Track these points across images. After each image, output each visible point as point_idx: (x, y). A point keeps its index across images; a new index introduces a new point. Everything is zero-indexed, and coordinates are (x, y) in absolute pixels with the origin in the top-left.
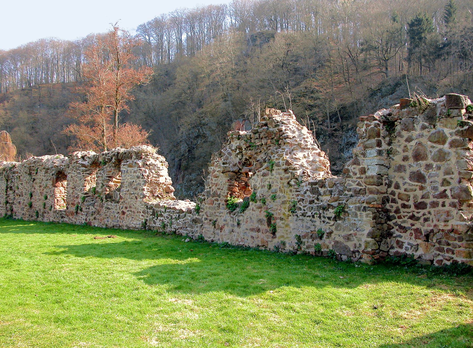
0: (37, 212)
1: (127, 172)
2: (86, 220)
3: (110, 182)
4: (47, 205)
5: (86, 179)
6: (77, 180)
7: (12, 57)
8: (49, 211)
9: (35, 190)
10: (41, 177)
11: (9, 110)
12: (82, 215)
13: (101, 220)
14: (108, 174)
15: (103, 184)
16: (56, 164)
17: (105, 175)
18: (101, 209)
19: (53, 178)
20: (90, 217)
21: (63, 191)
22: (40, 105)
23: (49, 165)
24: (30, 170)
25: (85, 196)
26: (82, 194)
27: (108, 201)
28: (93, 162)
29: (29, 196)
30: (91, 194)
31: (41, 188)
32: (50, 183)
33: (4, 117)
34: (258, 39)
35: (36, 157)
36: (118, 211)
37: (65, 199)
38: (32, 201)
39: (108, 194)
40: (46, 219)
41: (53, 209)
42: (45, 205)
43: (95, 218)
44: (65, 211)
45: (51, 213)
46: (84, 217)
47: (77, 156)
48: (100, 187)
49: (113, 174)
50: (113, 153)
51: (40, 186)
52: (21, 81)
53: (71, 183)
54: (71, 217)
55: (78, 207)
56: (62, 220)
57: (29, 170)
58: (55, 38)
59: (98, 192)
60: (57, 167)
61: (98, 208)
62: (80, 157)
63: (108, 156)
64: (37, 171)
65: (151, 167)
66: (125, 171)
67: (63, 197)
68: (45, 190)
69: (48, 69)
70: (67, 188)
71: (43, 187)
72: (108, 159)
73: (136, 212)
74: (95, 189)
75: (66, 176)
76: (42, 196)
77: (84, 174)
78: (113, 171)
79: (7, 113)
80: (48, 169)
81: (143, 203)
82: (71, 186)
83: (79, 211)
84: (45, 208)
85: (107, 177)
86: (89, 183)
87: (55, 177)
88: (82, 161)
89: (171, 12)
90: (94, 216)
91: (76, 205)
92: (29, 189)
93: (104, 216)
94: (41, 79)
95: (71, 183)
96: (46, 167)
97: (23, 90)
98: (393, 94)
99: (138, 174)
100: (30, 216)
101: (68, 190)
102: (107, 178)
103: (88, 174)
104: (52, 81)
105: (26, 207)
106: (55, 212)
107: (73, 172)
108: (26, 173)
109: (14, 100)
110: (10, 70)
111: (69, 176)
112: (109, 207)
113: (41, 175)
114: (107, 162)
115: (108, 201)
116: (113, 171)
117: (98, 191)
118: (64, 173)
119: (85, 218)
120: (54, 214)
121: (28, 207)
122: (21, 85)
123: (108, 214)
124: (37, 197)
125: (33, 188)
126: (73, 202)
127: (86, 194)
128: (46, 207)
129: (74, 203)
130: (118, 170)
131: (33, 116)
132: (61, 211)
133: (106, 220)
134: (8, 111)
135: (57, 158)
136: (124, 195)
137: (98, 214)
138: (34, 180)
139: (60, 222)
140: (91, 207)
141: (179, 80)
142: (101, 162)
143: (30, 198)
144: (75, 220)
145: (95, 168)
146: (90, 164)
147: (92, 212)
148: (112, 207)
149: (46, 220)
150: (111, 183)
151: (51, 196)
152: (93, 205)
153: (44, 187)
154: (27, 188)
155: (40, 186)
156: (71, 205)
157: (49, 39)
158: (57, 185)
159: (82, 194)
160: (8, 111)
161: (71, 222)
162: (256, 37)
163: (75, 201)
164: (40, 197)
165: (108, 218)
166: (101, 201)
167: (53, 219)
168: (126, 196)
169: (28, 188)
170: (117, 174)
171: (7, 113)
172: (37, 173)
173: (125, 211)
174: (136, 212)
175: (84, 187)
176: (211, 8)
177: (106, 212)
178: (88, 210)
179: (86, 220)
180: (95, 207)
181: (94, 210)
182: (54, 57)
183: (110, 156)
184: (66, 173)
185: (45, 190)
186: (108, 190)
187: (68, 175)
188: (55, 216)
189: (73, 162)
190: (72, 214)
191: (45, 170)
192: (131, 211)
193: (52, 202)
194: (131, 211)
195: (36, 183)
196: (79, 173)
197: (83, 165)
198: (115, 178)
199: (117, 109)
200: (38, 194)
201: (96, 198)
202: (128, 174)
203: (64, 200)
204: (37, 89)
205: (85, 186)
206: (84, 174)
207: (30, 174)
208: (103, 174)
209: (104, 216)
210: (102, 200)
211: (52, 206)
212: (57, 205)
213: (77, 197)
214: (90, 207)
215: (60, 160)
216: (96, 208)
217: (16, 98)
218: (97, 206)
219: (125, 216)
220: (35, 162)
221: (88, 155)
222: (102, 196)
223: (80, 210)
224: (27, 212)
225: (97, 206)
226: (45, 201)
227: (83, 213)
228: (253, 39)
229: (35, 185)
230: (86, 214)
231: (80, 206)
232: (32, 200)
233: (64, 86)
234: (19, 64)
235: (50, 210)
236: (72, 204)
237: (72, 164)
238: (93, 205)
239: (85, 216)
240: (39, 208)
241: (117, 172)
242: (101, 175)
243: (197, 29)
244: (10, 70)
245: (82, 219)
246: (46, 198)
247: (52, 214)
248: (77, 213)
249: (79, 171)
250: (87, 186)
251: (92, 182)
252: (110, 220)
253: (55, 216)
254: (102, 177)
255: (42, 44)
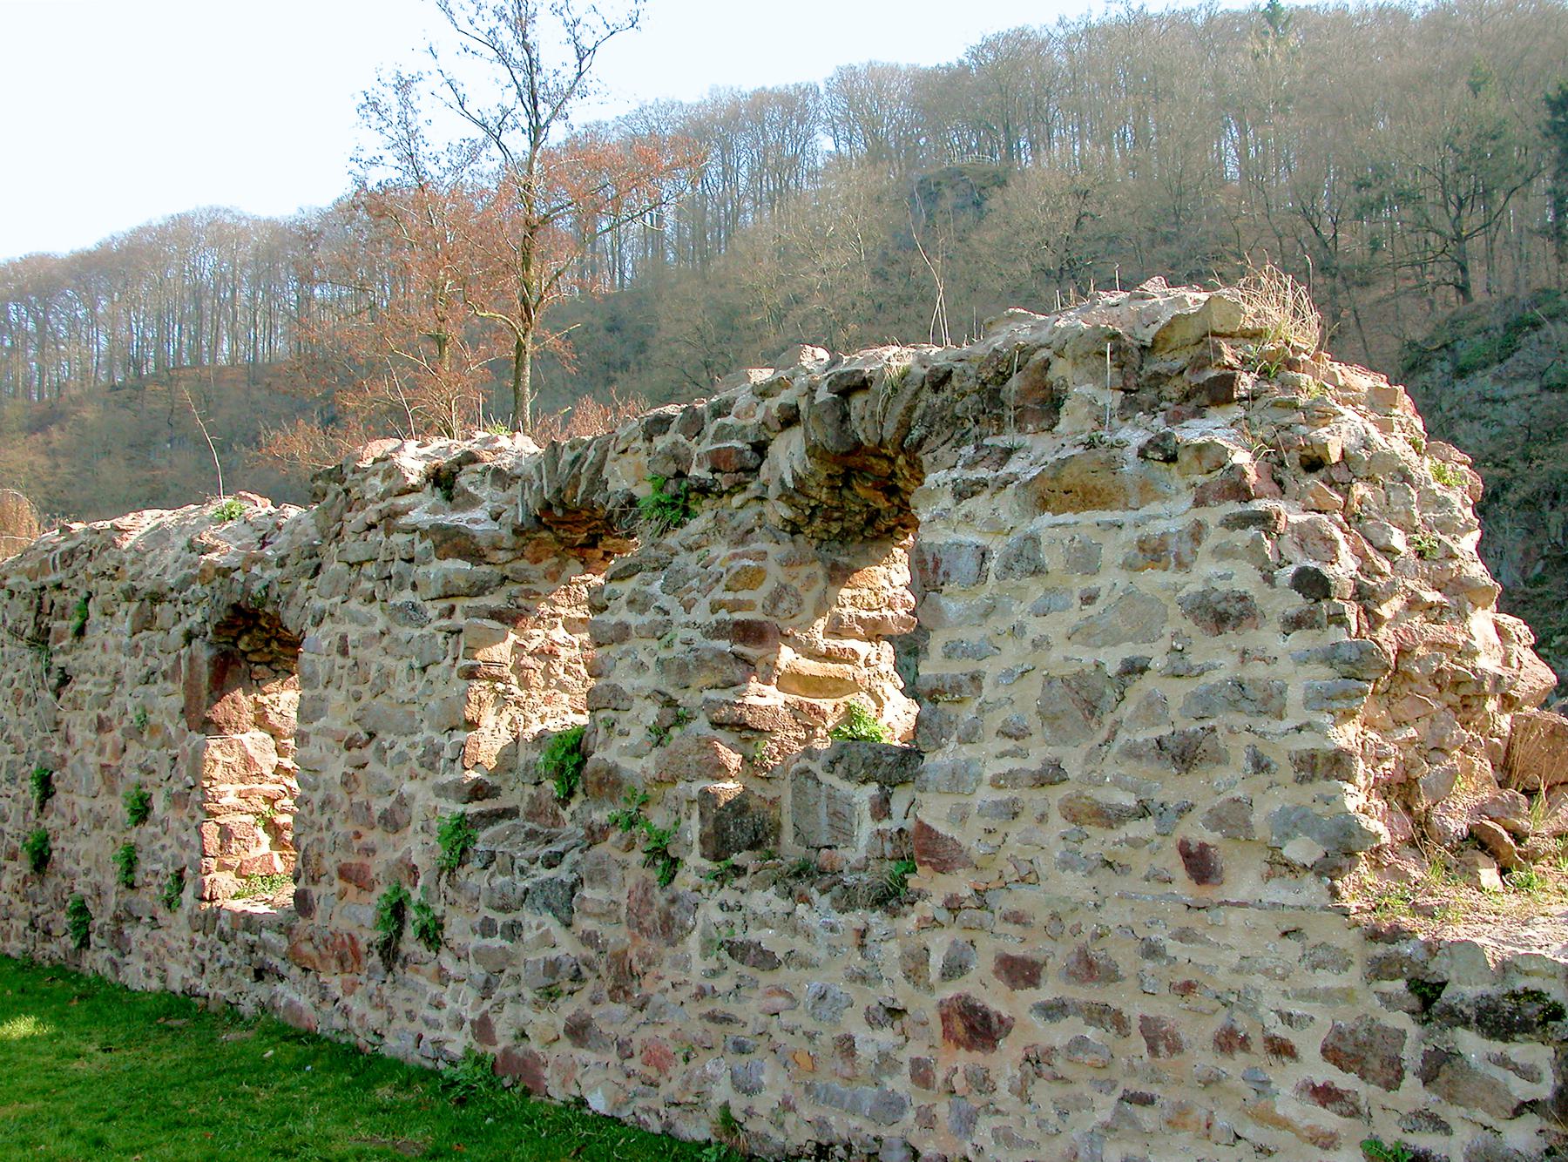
0: (81, 910)
1: (1027, 561)
2: (483, 1028)
3: (754, 685)
4: (145, 865)
5: (481, 655)
6: (387, 675)
7: (78, 277)
8: (161, 913)
9: (69, 753)
10: (105, 659)
11: (64, 455)
12: (442, 977)
13: (658, 1059)
14: (737, 606)
15: (670, 703)
16: (213, 556)
17: (701, 614)
18: (651, 946)
19: (191, 659)
20: (527, 1013)
21: (268, 759)
22: (170, 441)
23: (167, 567)
24: (39, 612)
25: (473, 808)
26: (441, 791)
27: (739, 871)
28: (547, 507)
29: (29, 791)
30: (516, 795)
31: (107, 738)
32: (168, 700)
33: (46, 479)
34: (947, 191)
35: (77, 527)
36: (898, 990)
37: (285, 819)
38: (47, 824)
39: (739, 806)
40: (142, 965)
41: (188, 896)
42: (130, 863)
43: (579, 1031)
44: (285, 929)
45: (178, 928)
46: (466, 1003)
47: (393, 472)
48: (638, 735)
49: (776, 598)
50: (774, 404)
51: (102, 726)
52: (110, 363)
53: (336, 698)
54: (335, 984)
55: (398, 910)
56: (262, 991)
57: (32, 614)
58: (227, 211)
59: (610, 783)
60: (224, 572)
61: (616, 936)
62: (414, 480)
63: (722, 433)
64: (85, 617)
65: (1360, 490)
66: (984, 555)
67: (266, 808)
68: (134, 749)
69: (201, 317)
70: (301, 738)
71: (117, 733)
72: (718, 462)
73: (1198, 1032)
74: (575, 748)
75: (293, 645)
76: (113, 791)
77: (459, 620)
78: (775, 574)
79: (57, 466)
80: (156, 598)
81: (1348, 940)
82: (338, 717)
83: (410, 944)
84: (131, 886)
85: (718, 631)
86: (502, 700)
87: (203, 652)
88: (434, 511)
89: (623, 116)
90: (567, 1008)
91: (382, 889)
92: (34, 740)
93: (689, 1020)
94: (178, 353)
95: (336, 698)
96: (145, 585)
97: (115, 388)
98: (1509, 362)
99: (1206, 573)
100: (33, 926)
101: (312, 751)
102: (724, 645)
103: (495, 615)
104: (214, 355)
105: (11, 865)
106: (208, 921)
107: (354, 604)
108: (16, 632)
109: (81, 423)
110: (74, 323)
111: (319, 640)
112: (767, 937)
113: (111, 641)
114: (704, 490)
115: (739, 871)
116: (775, 574)
117: (613, 770)
118: (275, 620)
119: (471, 1015)
120: (199, 937)
121: (24, 866)
122: (110, 374)
123: (750, 1010)
124: (84, 803)
125: (56, 738)
126: (354, 860)
127: (478, 791)
128: (139, 877)
129: (363, 869)
130: (819, 570)
131: (148, 475)
132: (248, 922)
133: (714, 1066)
134: (61, 460)
135: (226, 517)
136: (977, 825)
137: (619, 992)
138: (65, 680)
139: (247, 1008)
140: (535, 921)
141: (669, 336)
142: (632, 501)
143: (35, 804)
144: (375, 1018)
145: (549, 563)
146: (517, 532)
147: (553, 967)
148: (800, 944)
149: (136, 974)
150: (765, 698)
151: (178, 800)
152: (564, 902)
153: (125, 732)
154: (20, 732)
155: (102, 726)
156: (339, 884)
157: (205, 216)
158: (220, 711)
159: (441, 791)
160: (61, 460)
161: (339, 1022)
162: (938, 184)
163: (370, 851)
164: (98, 804)
165: (741, 1048)
166: (653, 875)
167: (188, 973)
168: (1016, 830)
169: (28, 736)
170: (810, 599)
171: (57, 466)
172: (80, 632)
173: (997, 999)
174: (1198, 1032)
175: (459, 736)
176: (761, 101)
177: (724, 984)
178: (497, 942)
179: (483, 1028)
180: (586, 924)
181: (567, 947)
182: (223, 275)
183: (741, 432)
184: (290, 617)
185: (134, 749)
186: (734, 760)
187: (311, 633)
188: (206, 955)
189: (356, 519)
190: (347, 955)
191: (135, 606)
192: (1102, 1015)
193: (184, 845)
194: (1102, 1015)
195: (73, 701)
196: (412, 613)
197: (453, 542)
198: (797, 645)
199: (530, 336)
200: (91, 781)
201: (595, 835)
202: (1035, 590)
203: (272, 828)
204: (163, 384)
205: (472, 725)
206: (459, 620)
207: (41, 639)
208: (665, 601)
209: (689, 1020)
210: (665, 859)
211: (179, 877)
212: (223, 867)
213: (392, 822)
214: (527, 916)
215: (247, 530)
216: (589, 939)
217: (90, 414)
218: (607, 914)
219: (1005, 1061)
220: (72, 553)
221: (487, 456)
222: (659, 818)
223: (423, 932)
224: (16, 900)
225: (607, 914)
226: (133, 836)
227: (447, 960)
228: (930, 192)
229: (66, 716)
230: (479, 972)
231: (416, 895)
232: (52, 822)
233: (255, 374)
234: (103, 303)
235: (169, 903)
236: (344, 873)
237: (349, 539)
238: (564, 902)
239: (470, 994)
240: (95, 877)
241: (811, 579)
242: (651, 616)
243: (714, 171)
244: (74, 323)
245: (442, 1016)
246: (142, 811)
247: (186, 934)
248: (389, 952)
249: (407, 596)
250: (488, 719)
251: (525, 684)
252: (774, 1082)
253: (206, 955)
254: (660, 632)
255: (181, 232)
